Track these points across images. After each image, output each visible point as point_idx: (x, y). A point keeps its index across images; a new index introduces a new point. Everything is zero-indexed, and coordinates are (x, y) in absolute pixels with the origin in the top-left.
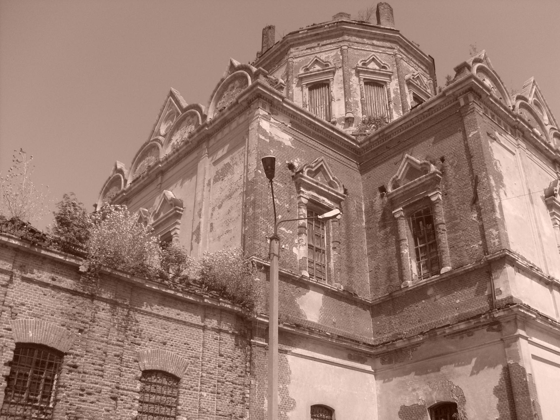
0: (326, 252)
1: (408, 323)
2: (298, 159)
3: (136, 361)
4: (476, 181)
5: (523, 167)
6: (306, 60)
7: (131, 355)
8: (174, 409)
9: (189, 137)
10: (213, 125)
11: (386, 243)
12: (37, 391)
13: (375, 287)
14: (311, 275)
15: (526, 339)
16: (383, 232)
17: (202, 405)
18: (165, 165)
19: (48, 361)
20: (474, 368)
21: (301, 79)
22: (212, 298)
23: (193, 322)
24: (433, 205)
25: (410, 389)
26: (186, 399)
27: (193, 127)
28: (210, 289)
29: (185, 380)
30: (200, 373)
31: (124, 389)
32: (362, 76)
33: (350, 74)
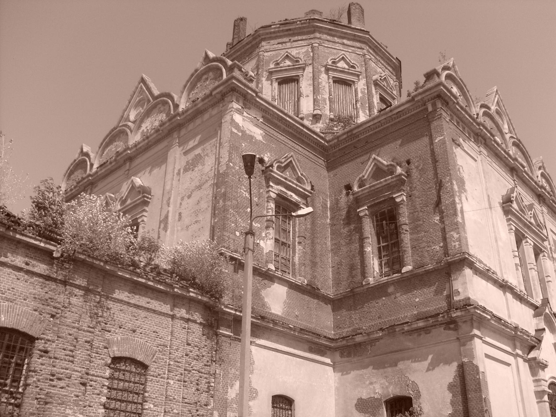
0: (291, 246)
1: (369, 318)
2: (269, 154)
3: (106, 348)
4: (440, 185)
5: (484, 173)
6: (277, 54)
7: (101, 342)
8: (141, 396)
9: (161, 126)
10: (185, 115)
11: (350, 240)
12: (7, 375)
13: (337, 282)
14: (277, 269)
15: (481, 338)
16: (347, 229)
17: (169, 393)
18: (134, 152)
19: (19, 345)
20: (429, 364)
21: (271, 73)
22: (182, 288)
23: (163, 311)
24: (397, 205)
25: (368, 382)
26: (154, 387)
27: (164, 115)
28: (182, 278)
29: (153, 368)
30: (168, 361)
31: (93, 375)
32: (331, 74)
33: (320, 72)
